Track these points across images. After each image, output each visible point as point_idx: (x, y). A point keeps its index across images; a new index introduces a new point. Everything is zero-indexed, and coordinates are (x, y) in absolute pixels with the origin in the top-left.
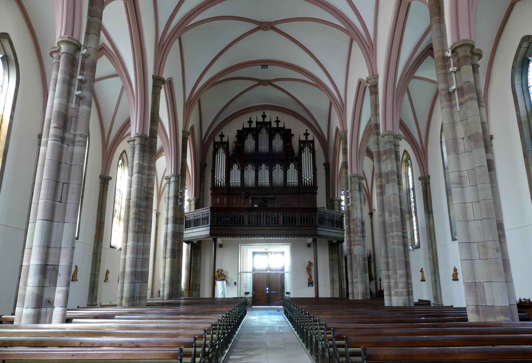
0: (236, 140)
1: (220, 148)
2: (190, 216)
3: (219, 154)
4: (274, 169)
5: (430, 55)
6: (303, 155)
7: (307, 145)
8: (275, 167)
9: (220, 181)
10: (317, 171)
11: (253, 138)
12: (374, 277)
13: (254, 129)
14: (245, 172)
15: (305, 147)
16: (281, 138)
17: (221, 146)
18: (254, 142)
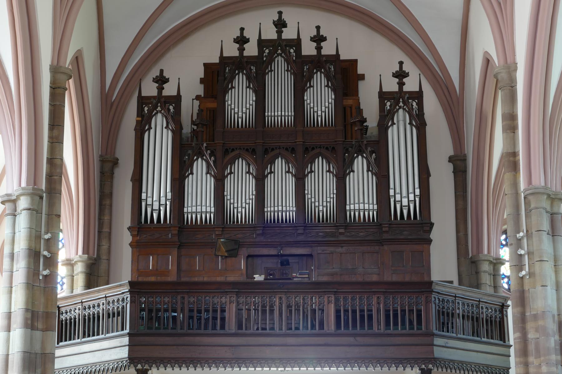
3: (152, 131)
4: (308, 173)
6: (392, 133)
13: (251, 60)
14: (227, 182)
16: (327, 86)
18: (251, 97)
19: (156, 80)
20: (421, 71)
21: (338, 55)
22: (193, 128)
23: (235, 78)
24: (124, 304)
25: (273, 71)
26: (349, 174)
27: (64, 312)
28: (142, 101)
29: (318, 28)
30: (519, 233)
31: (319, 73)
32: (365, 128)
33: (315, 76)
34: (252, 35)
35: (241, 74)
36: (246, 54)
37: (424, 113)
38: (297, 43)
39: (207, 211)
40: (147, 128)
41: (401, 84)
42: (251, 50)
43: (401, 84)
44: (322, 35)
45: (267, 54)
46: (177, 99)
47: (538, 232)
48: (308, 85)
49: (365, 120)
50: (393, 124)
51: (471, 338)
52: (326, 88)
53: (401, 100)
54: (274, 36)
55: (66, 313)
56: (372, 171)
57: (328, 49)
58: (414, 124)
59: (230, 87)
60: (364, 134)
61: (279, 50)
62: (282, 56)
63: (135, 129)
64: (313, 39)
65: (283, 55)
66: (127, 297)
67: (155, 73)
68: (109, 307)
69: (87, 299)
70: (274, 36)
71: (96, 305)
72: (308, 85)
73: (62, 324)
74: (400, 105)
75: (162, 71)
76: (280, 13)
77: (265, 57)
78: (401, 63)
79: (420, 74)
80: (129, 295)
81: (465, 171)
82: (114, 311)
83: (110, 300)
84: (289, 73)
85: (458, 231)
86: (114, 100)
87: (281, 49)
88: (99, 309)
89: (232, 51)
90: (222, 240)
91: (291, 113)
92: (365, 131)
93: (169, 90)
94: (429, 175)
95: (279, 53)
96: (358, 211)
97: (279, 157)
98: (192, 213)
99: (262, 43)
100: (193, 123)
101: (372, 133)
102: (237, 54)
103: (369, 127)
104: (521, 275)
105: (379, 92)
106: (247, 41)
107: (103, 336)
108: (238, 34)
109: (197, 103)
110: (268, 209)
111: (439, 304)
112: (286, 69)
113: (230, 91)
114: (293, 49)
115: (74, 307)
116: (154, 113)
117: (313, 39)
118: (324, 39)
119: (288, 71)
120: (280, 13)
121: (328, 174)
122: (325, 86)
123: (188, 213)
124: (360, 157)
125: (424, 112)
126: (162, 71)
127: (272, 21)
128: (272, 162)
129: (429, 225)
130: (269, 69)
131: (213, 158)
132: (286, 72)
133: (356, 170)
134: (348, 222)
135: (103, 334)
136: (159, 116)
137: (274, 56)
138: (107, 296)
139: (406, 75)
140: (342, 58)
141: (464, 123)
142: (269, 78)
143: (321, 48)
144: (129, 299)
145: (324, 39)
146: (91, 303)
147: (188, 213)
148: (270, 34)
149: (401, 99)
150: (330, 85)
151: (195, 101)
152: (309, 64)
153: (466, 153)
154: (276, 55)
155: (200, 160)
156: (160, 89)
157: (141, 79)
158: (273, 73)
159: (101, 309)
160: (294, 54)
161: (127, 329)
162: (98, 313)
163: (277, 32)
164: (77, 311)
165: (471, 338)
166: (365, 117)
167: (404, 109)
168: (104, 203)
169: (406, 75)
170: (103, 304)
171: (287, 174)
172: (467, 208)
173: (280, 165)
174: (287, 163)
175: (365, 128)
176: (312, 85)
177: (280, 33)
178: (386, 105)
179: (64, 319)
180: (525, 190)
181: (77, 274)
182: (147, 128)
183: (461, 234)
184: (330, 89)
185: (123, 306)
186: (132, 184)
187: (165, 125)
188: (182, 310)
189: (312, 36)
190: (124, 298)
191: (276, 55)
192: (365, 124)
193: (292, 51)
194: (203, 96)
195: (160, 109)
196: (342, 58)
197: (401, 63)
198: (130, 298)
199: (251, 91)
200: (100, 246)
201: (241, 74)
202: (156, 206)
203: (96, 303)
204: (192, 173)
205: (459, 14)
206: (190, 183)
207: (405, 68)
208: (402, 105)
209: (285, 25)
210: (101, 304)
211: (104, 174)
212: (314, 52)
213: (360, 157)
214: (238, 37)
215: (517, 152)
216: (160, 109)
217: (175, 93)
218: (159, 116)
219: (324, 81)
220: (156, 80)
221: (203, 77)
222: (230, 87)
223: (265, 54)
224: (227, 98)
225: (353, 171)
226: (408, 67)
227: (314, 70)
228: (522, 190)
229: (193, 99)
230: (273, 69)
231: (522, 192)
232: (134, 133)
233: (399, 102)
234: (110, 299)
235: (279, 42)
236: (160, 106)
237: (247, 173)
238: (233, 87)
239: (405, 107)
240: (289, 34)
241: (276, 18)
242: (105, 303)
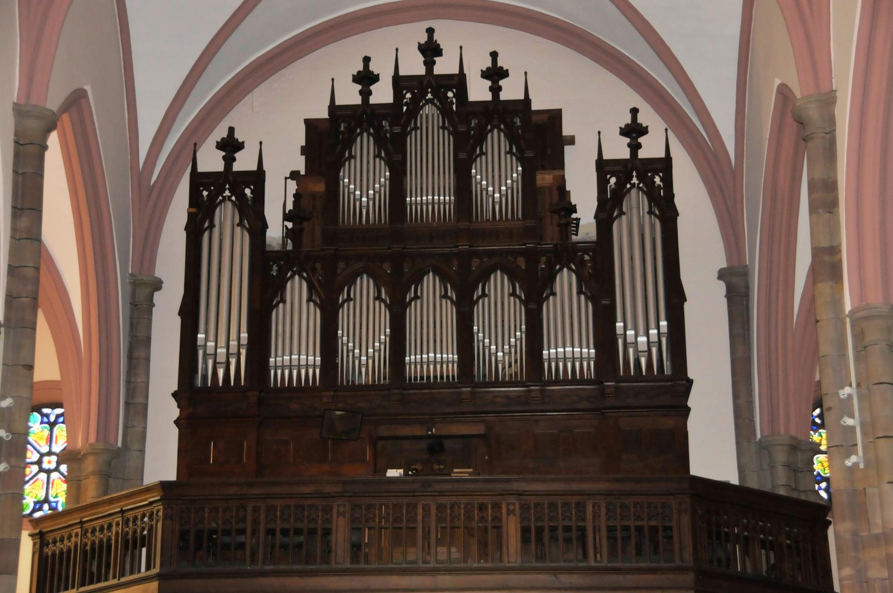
3: (216, 231)
6: (620, 229)
7: (635, 180)
16: (510, 152)
19: (221, 146)
20: (668, 126)
21: (527, 101)
22: (286, 226)
23: (355, 140)
24: (152, 522)
25: (418, 128)
26: (547, 297)
27: (51, 541)
28: (198, 180)
29: (494, 55)
30: (843, 388)
31: (496, 131)
32: (574, 224)
33: (489, 136)
34: (383, 68)
35: (365, 135)
36: (373, 100)
37: (674, 195)
38: (459, 81)
39: (309, 363)
40: (206, 225)
41: (635, 147)
42: (382, 94)
43: (635, 147)
44: (501, 68)
45: (408, 101)
46: (257, 178)
47: (877, 385)
48: (478, 152)
49: (574, 209)
50: (622, 213)
52: (509, 156)
53: (634, 174)
54: (421, 70)
55: (55, 542)
57: (511, 91)
58: (657, 212)
59: (347, 155)
60: (574, 234)
61: (428, 93)
62: (434, 104)
63: (187, 228)
64: (486, 75)
65: (435, 101)
66: (158, 511)
67: (220, 133)
68: (128, 529)
69: (90, 516)
70: (421, 70)
71: (98, 529)
72: (478, 152)
73: (46, 561)
74: (632, 182)
75: (231, 130)
76: (431, 31)
77: (405, 105)
78: (634, 112)
79: (666, 130)
80: (161, 507)
81: (746, 295)
82: (136, 535)
83: (129, 516)
84: (446, 132)
85: (736, 396)
86: (155, 182)
88: (110, 534)
89: (350, 96)
90: (338, 413)
91: (449, 198)
92: (575, 229)
93: (244, 162)
94: (683, 298)
95: (429, 99)
96: (563, 360)
97: (430, 271)
98: (283, 367)
99: (400, 83)
100: (287, 217)
101: (588, 234)
102: (357, 100)
103: (581, 223)
104: (849, 463)
105: (596, 160)
106: (375, 79)
107: (115, 581)
108: (360, 67)
109: (292, 186)
111: (440, 515)
112: (441, 124)
113: (347, 163)
114: (453, 92)
115: (68, 532)
116: (218, 201)
117: (486, 75)
118: (504, 74)
119: (444, 128)
120: (431, 31)
121: (512, 298)
122: (507, 153)
123: (283, 368)
124: (565, 270)
125: (674, 192)
126: (231, 130)
127: (417, 45)
128: (419, 281)
129: (684, 382)
130: (413, 126)
132: (441, 131)
134: (546, 379)
135: (114, 577)
137: (421, 104)
138: (124, 509)
139: (644, 131)
140: (534, 107)
141: (743, 214)
142: (411, 142)
143: (500, 88)
144: (161, 513)
145: (504, 74)
146: (97, 523)
147: (283, 368)
148: (414, 66)
150: (514, 150)
151: (289, 181)
152: (479, 116)
153: (748, 263)
154: (424, 101)
156: (229, 160)
157: (195, 144)
158: (419, 131)
159: (114, 533)
160: (454, 100)
161: (156, 567)
162: (109, 539)
163: (425, 63)
164: (73, 539)
166: (573, 204)
167: (639, 189)
168: (136, 355)
169: (644, 131)
170: (118, 524)
171: (444, 301)
172: (750, 356)
175: (574, 224)
176: (484, 150)
177: (429, 64)
178: (610, 183)
179: (50, 554)
180: (852, 312)
181: (87, 477)
182: (206, 225)
183: (742, 401)
184: (514, 158)
185: (152, 526)
186: (180, 320)
187: (237, 220)
188: (254, 532)
189: (484, 69)
190: (153, 512)
191: (424, 101)
192: (574, 216)
193: (450, 94)
194: (303, 172)
195: (229, 194)
196: (534, 107)
197: (634, 112)
198: (163, 513)
199: (383, 163)
200: (128, 427)
201: (365, 135)
202: (221, 358)
203: (105, 522)
204: (283, 301)
206: (280, 317)
207: (641, 119)
208: (637, 182)
209: (438, 52)
210: (114, 524)
211: (138, 306)
212: (488, 96)
213: (565, 270)
214: (359, 72)
215: (837, 246)
216: (229, 194)
217: (254, 167)
219: (505, 145)
220: (221, 146)
221: (304, 144)
222: (347, 155)
223: (405, 100)
224: (341, 174)
225: (554, 294)
226: (647, 117)
227: (488, 126)
228: (847, 312)
229: (286, 178)
230: (419, 125)
231: (847, 316)
232: (184, 235)
234: (130, 515)
235: (429, 80)
236: (229, 189)
237: (375, 299)
238: (351, 157)
239: (641, 185)
240: (445, 66)
241: (424, 38)
242: (121, 523)
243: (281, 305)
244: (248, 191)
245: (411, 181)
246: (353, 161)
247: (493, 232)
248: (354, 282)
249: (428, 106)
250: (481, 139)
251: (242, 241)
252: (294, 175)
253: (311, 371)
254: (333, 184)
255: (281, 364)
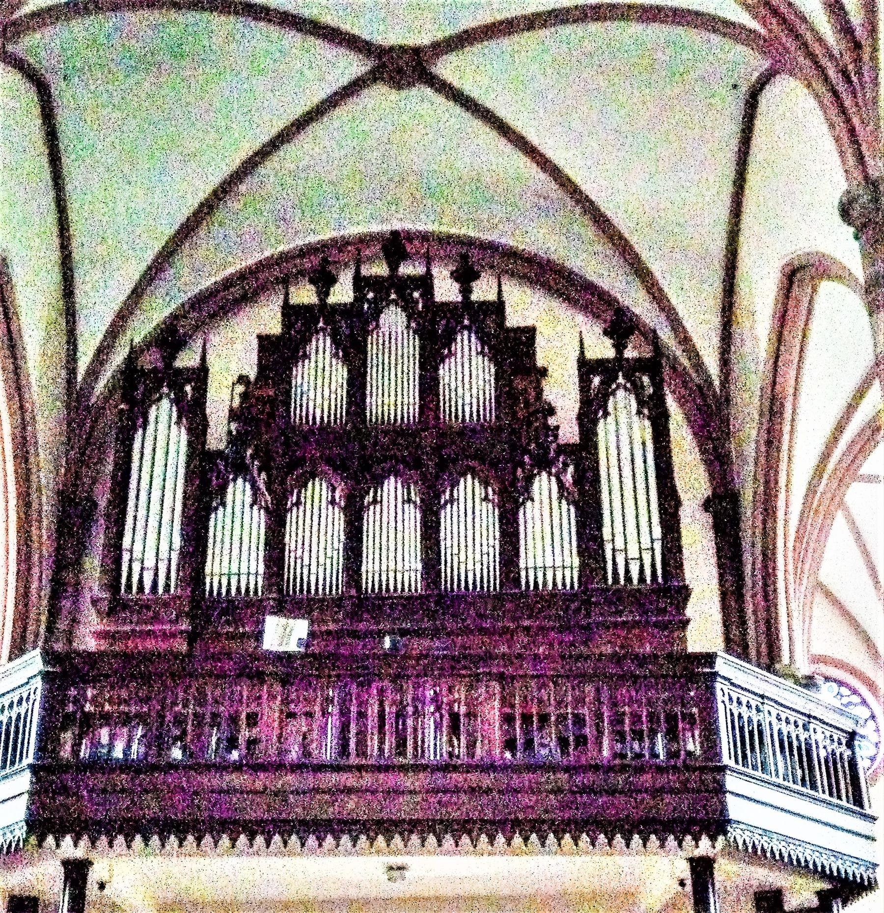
0: (252, 373)
1: (160, 399)
2: (18, 692)
3: (151, 428)
4: (446, 503)
5: (278, 338)
6: (605, 431)
7: (621, 380)
8: (452, 495)
9: (150, 563)
10: (681, 509)
11: (483, 348)
12: (379, 499)
13: (343, 310)
14: (291, 518)
15: (613, 393)
16: (482, 353)
17: (165, 390)
18: (340, 373)
51: (799, 787)
56: (567, 499)
87: (396, 293)
110: (370, 567)
128: (379, 482)
131: (263, 475)
133: (536, 497)
136: (165, 404)
149: (620, 374)
155: (240, 481)
165: (799, 787)
171: (406, 506)
173: (391, 488)
174: (406, 484)
184: (486, 358)
205: (718, 245)
218: (165, 404)
233: (617, 378)
243: (221, 508)
244: (188, 388)
245: (373, 377)
246: (307, 361)
247: (467, 432)
248: (306, 486)
249: (313, 484)
250: (449, 339)
251: (180, 439)
252: (242, 379)
253: (252, 579)
254: (286, 381)
255: (542, 565)
